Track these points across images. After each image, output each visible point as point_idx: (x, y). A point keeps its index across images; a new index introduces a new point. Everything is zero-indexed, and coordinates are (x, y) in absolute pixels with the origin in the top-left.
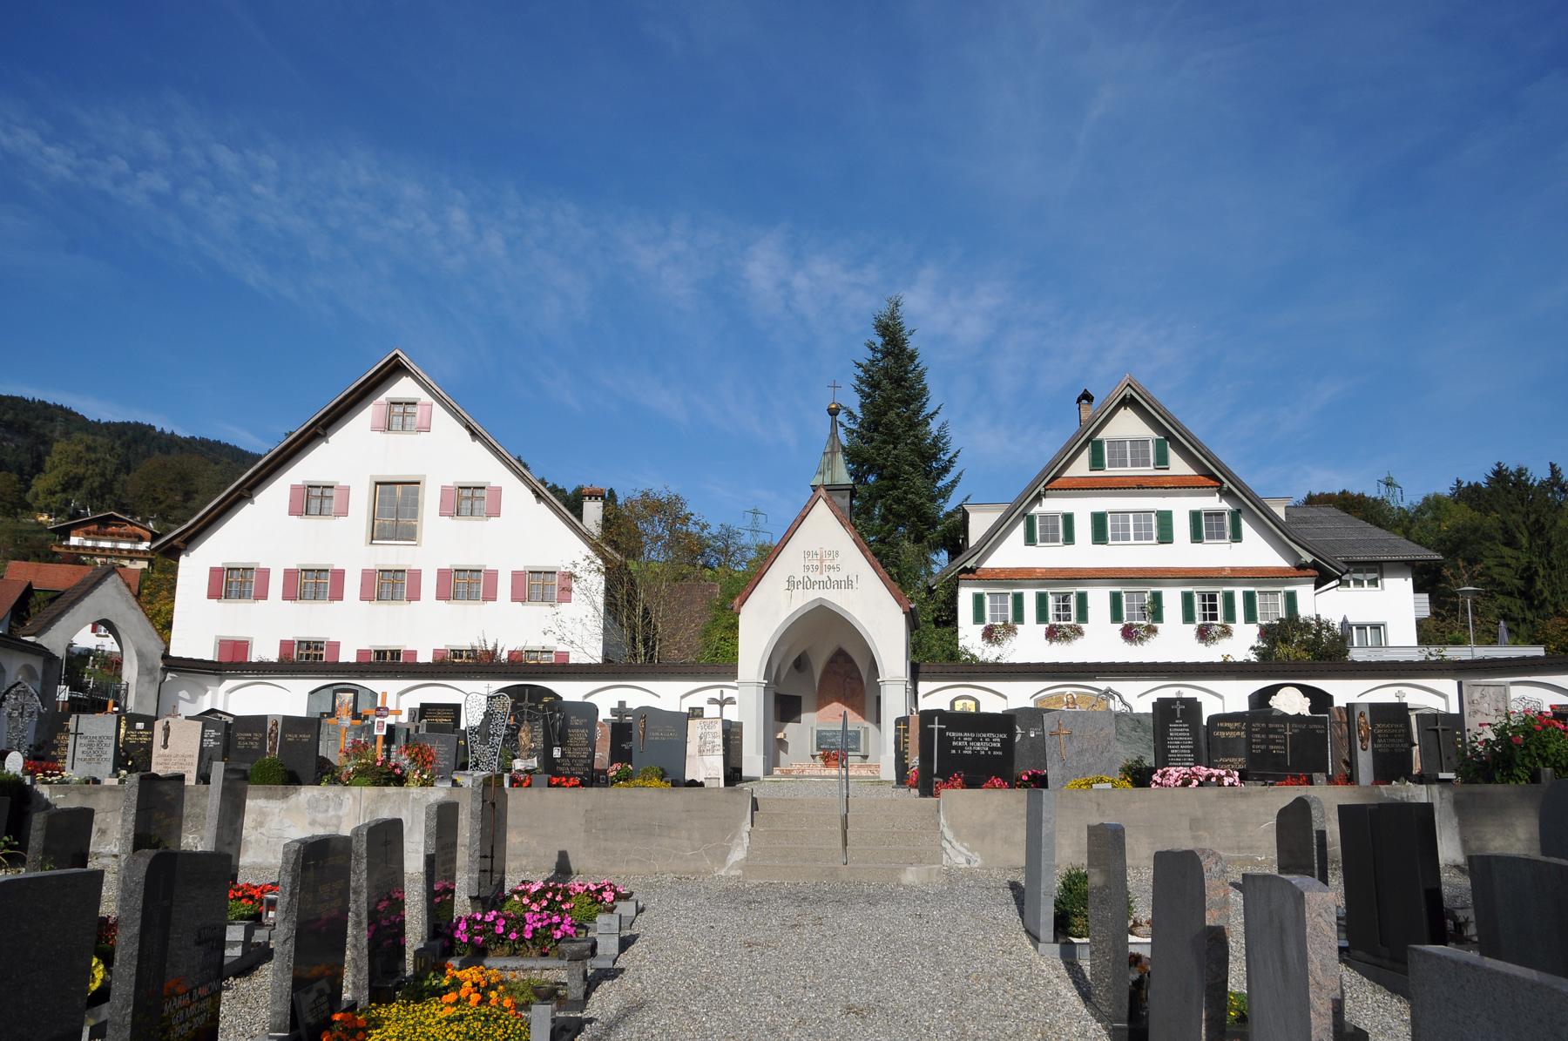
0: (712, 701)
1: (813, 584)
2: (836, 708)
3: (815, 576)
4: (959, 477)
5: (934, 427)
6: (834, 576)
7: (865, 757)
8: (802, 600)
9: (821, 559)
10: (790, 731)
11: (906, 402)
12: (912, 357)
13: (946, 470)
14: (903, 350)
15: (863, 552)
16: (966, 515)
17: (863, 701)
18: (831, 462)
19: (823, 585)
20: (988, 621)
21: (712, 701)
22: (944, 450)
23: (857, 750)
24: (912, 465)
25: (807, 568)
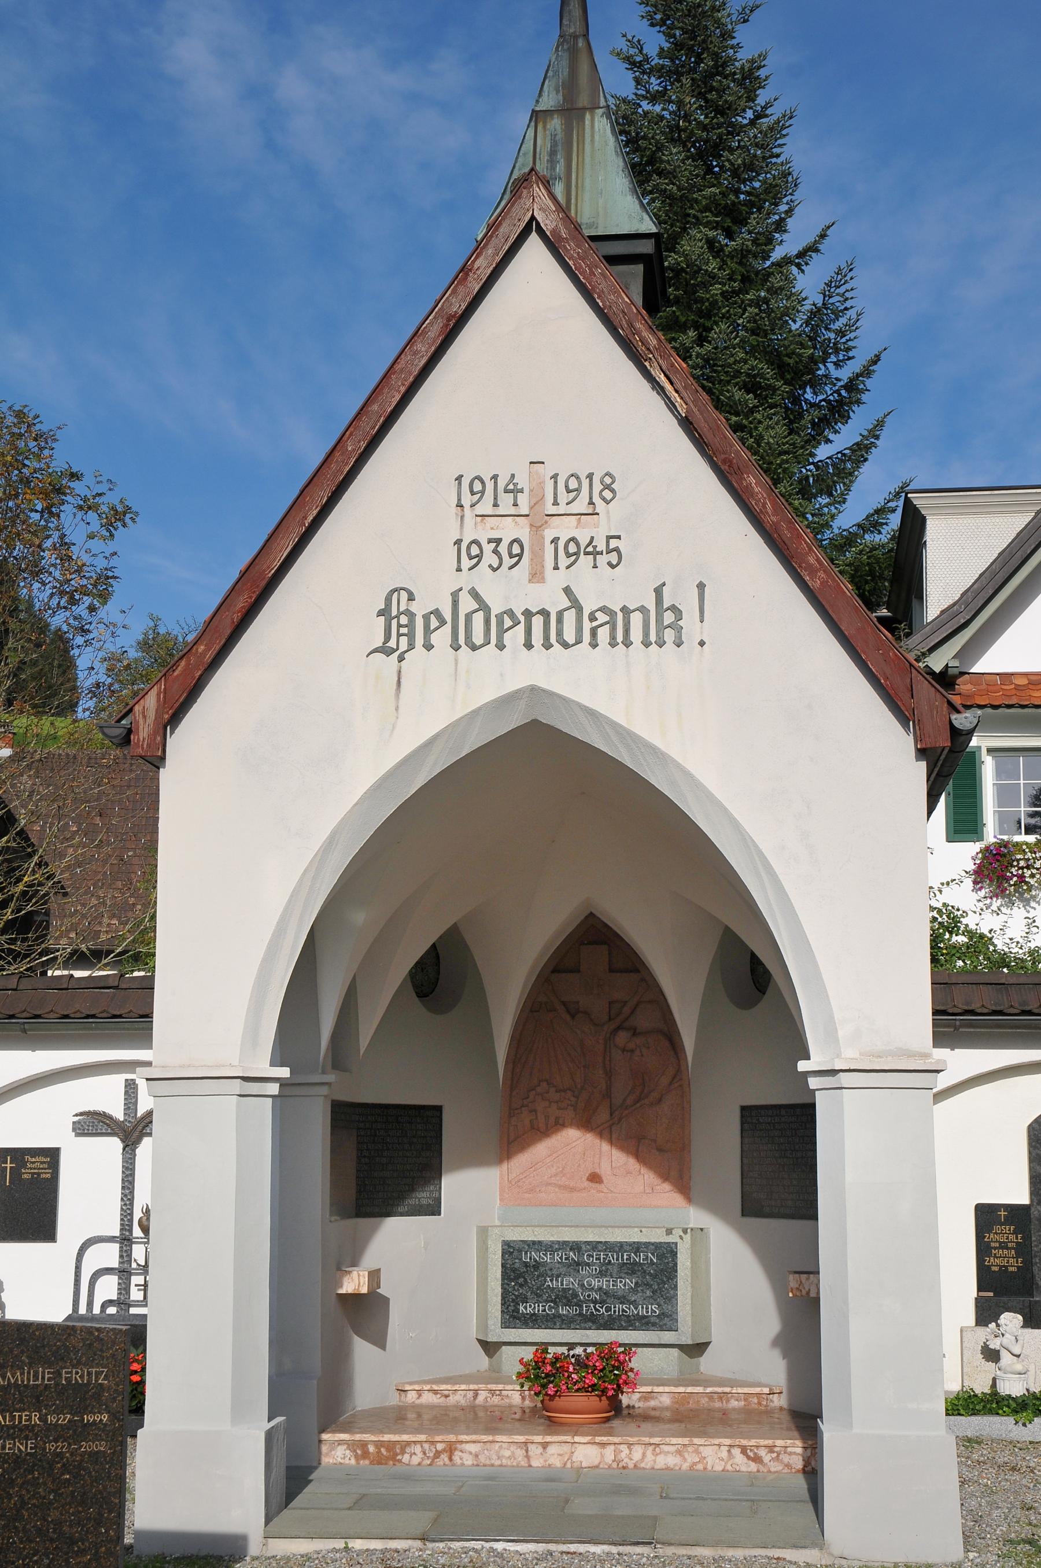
0: (92, 1124)
1: (499, 625)
2: (572, 1148)
3: (506, 590)
4: (874, 432)
5: (809, 284)
6: (595, 585)
7: (696, 1349)
8: (451, 697)
9: (534, 516)
10: (396, 1244)
11: (733, 216)
12: (750, 79)
13: (838, 411)
14: (721, 66)
15: (727, 475)
16: (914, 525)
17: (682, 1116)
18: (567, 146)
19: (543, 628)
20: (991, 834)
21: (92, 1124)
22: (841, 351)
23: (666, 1320)
24: (752, 386)
25: (470, 553)
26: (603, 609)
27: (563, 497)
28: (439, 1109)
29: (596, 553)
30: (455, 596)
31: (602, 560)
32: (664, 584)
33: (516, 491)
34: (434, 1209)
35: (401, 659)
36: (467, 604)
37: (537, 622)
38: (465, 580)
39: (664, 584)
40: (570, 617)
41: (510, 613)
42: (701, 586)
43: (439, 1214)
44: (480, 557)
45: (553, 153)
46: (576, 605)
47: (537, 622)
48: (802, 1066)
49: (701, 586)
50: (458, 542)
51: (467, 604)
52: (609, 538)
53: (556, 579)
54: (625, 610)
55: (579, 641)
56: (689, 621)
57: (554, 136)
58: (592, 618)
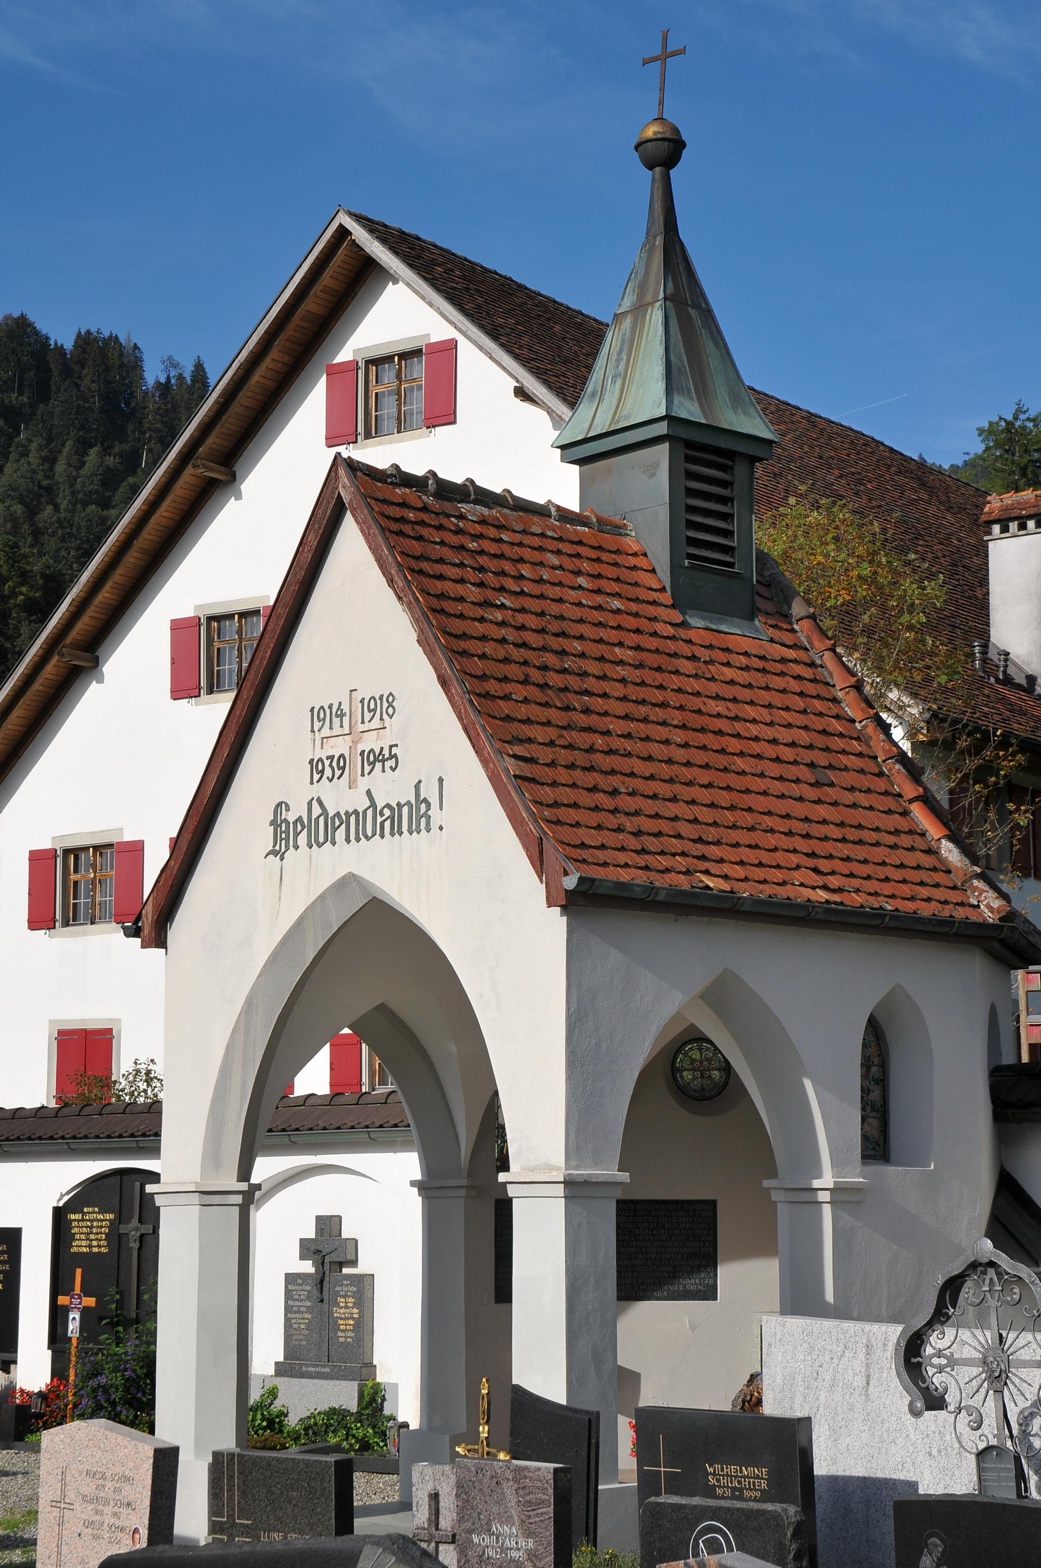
19: (356, 825)
26: (388, 806)
27: (368, 716)
28: (714, 1203)
29: (383, 761)
30: (310, 804)
31: (388, 764)
32: (420, 782)
33: (341, 716)
34: (709, 1293)
35: (282, 859)
36: (316, 810)
37: (353, 818)
38: (314, 791)
39: (420, 782)
40: (370, 812)
41: (338, 814)
42: (441, 780)
43: (715, 1299)
44: (322, 772)
45: (621, 351)
46: (373, 804)
47: (353, 818)
48: (502, 1177)
49: (441, 780)
50: (312, 760)
51: (316, 810)
52: (391, 747)
53: (364, 783)
54: (398, 804)
55: (374, 834)
56: (434, 812)
57: (624, 335)
58: (382, 814)
